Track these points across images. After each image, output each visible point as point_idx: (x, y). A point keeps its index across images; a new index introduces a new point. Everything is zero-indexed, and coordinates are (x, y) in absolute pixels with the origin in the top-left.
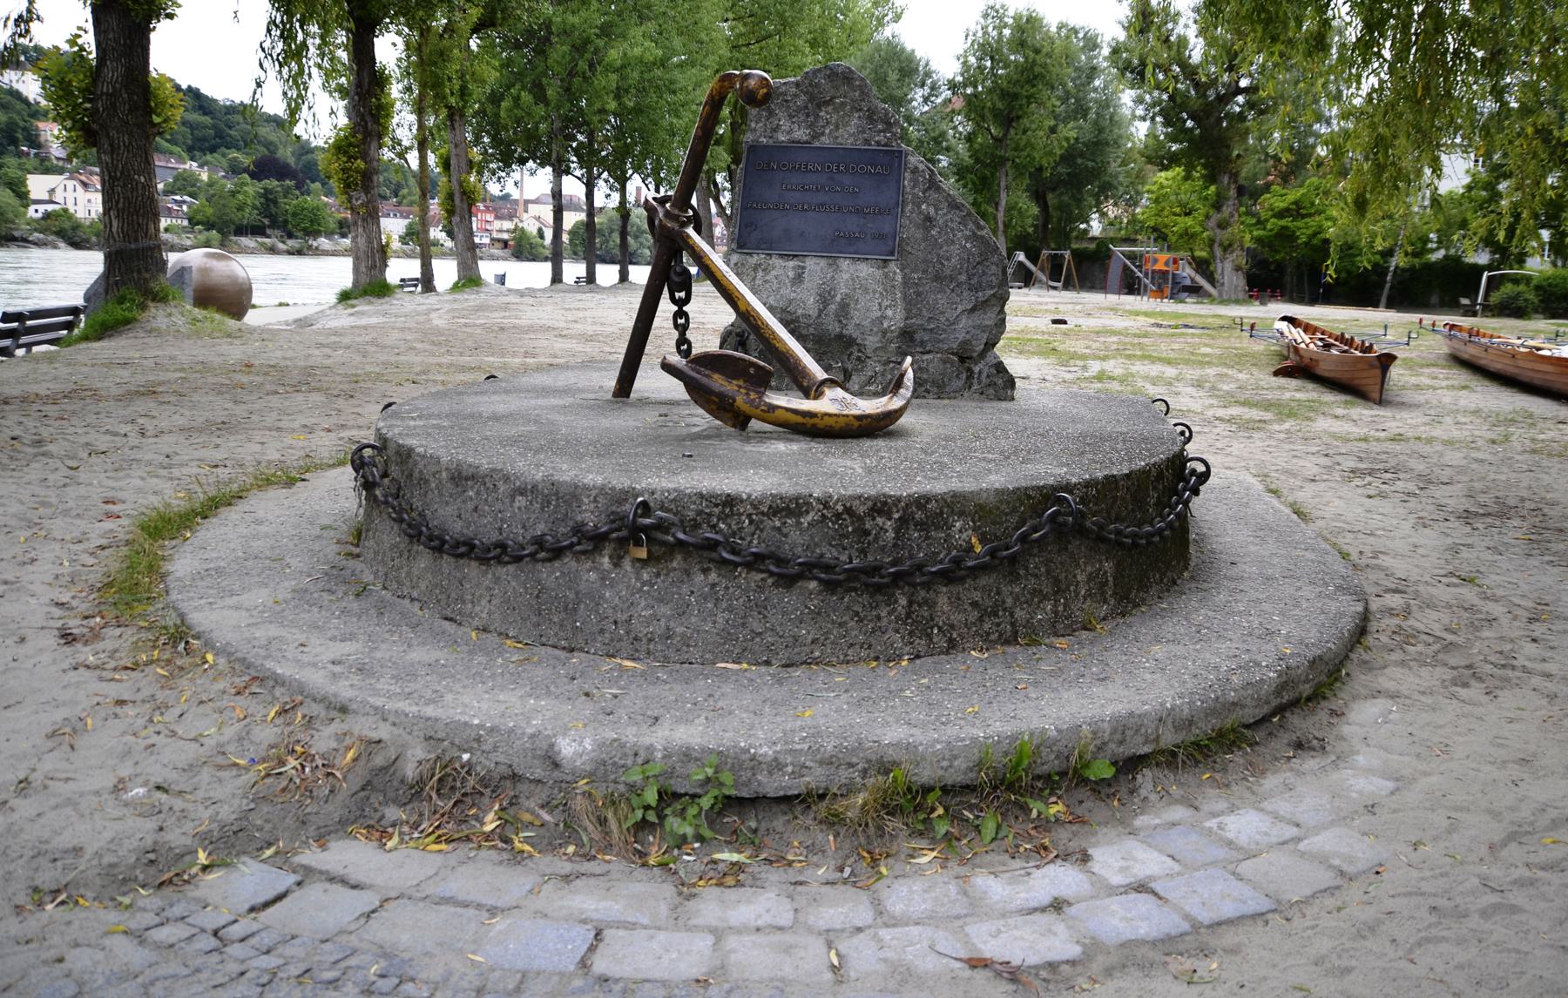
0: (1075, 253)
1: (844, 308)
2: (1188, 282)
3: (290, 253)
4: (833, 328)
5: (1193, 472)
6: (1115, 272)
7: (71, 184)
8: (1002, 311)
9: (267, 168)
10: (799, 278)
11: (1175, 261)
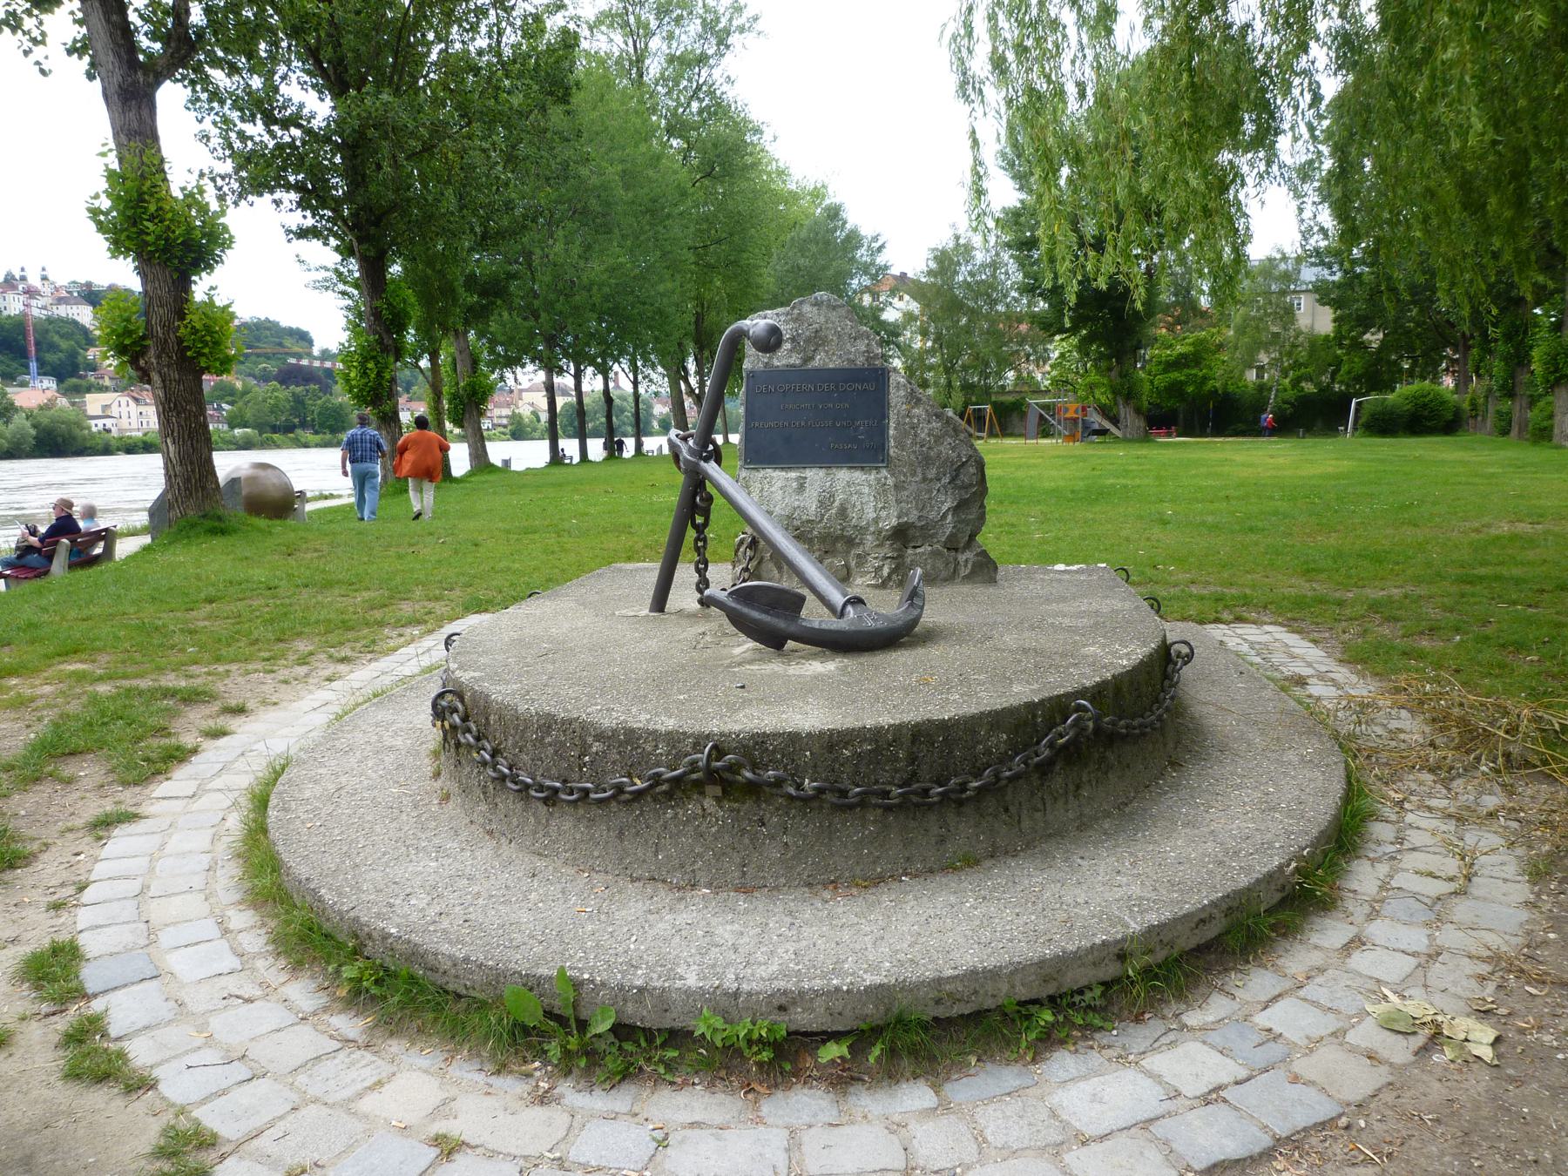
0: (995, 405)
1: (843, 512)
2: (1096, 427)
3: (317, 446)
4: (837, 529)
5: (1179, 655)
6: (1032, 420)
7: (124, 400)
8: (982, 506)
9: (290, 376)
10: (801, 488)
11: (1084, 409)
